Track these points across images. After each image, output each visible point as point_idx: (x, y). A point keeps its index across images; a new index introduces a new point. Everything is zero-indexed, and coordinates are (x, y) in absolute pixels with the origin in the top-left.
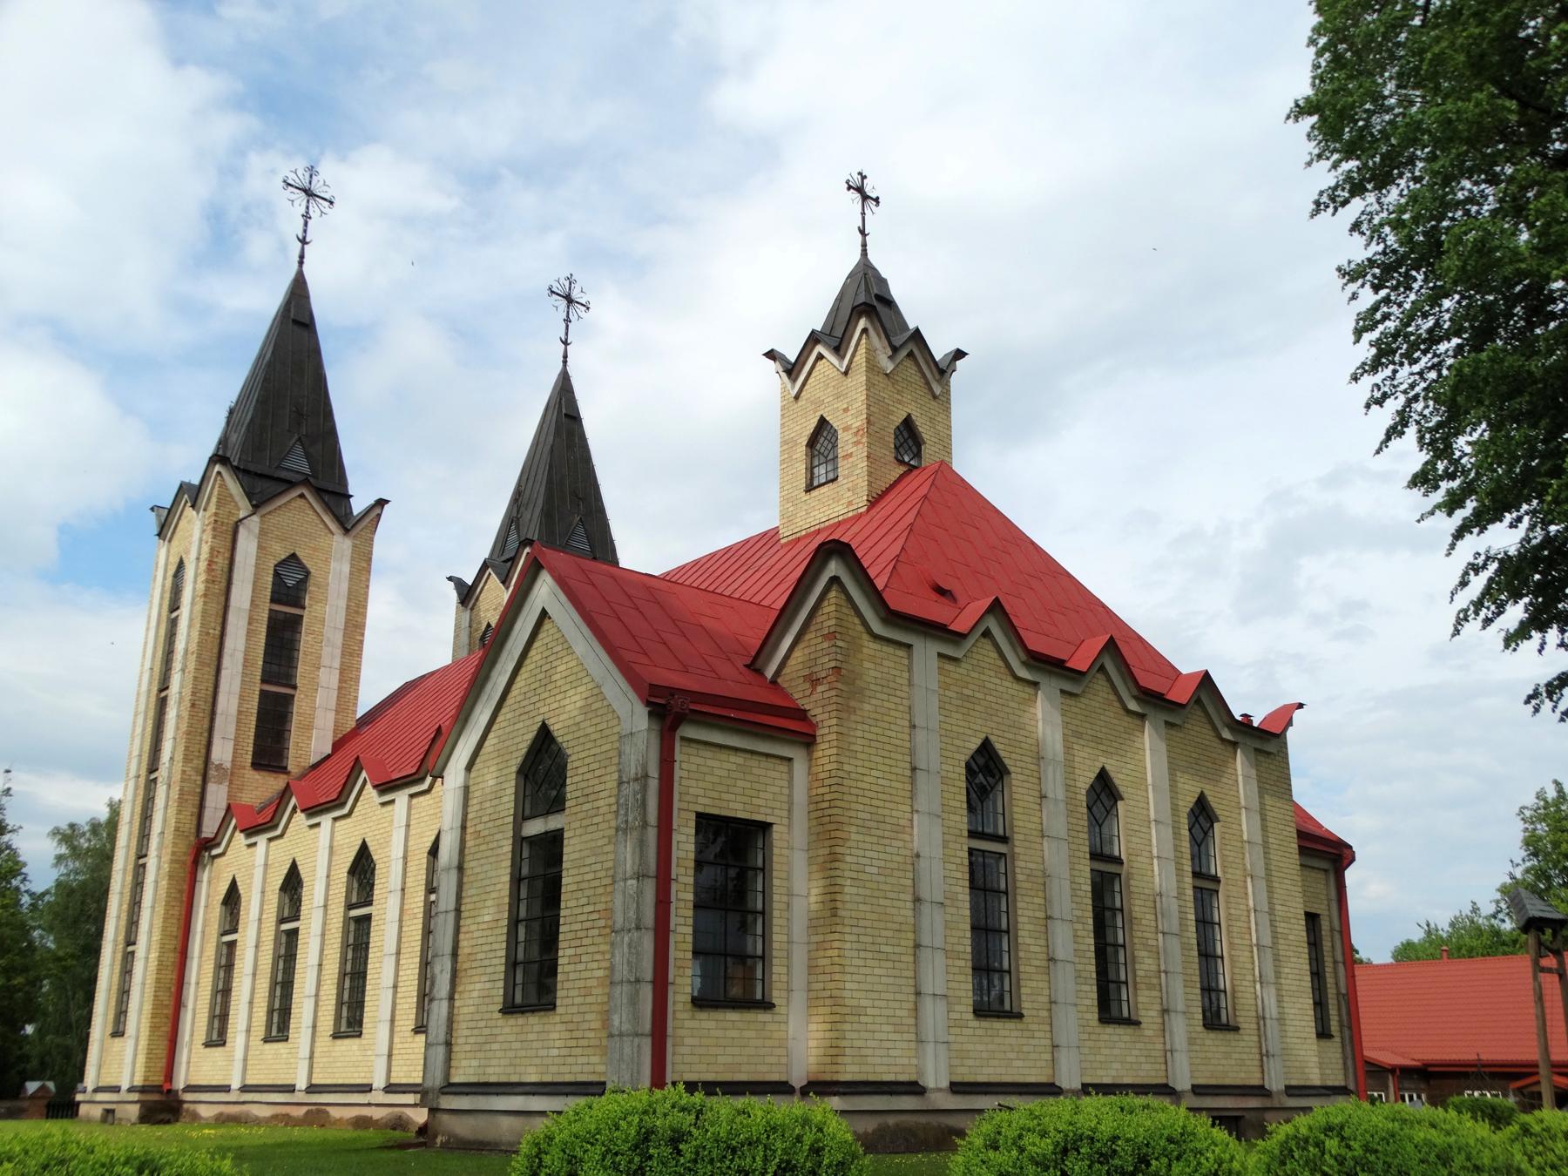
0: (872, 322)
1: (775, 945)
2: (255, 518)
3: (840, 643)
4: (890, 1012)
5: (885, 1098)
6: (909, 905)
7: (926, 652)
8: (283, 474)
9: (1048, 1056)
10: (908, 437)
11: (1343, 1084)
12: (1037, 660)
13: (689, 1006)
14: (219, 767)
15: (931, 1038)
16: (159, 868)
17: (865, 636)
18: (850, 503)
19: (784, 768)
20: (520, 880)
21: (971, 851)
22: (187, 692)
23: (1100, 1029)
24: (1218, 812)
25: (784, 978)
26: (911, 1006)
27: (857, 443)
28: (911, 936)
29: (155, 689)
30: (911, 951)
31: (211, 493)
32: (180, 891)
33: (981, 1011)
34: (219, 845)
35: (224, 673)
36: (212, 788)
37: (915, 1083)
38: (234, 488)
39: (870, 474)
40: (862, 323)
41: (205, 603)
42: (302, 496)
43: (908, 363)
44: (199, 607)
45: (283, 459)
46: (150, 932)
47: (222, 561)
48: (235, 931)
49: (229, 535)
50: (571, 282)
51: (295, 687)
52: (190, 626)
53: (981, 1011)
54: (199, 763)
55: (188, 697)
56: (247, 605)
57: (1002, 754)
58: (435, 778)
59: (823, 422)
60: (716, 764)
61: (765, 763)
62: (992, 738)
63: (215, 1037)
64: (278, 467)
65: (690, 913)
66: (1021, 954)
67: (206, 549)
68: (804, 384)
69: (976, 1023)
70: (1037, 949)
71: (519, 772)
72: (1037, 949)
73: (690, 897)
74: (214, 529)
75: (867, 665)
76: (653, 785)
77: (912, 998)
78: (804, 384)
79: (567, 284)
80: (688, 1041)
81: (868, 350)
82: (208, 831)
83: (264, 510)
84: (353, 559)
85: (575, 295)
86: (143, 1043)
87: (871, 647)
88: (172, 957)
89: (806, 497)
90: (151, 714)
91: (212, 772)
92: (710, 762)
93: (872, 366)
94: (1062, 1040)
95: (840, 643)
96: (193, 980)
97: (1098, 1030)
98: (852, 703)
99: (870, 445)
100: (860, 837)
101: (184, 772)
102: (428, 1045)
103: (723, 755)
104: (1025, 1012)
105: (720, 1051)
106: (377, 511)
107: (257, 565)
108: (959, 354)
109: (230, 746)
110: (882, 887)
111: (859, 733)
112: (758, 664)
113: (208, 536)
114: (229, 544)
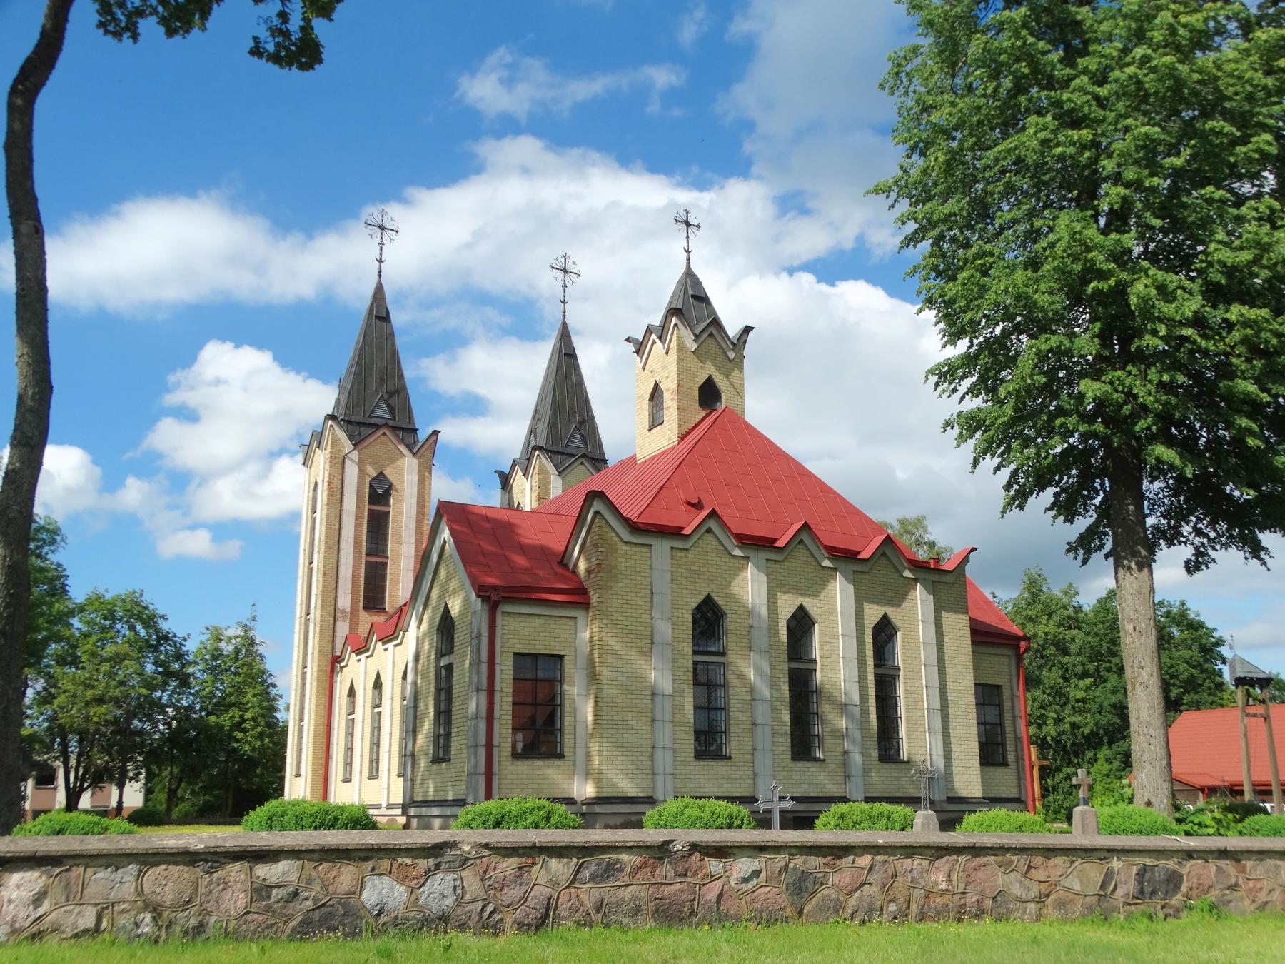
0: (680, 320)
1: (566, 723)
2: (355, 452)
3: (601, 549)
4: (635, 758)
5: (628, 806)
6: (649, 697)
7: (662, 547)
8: (373, 421)
9: (751, 781)
10: (709, 394)
11: (1017, 796)
12: (747, 541)
13: (510, 758)
14: (343, 611)
15: (661, 771)
16: (312, 675)
17: (619, 543)
18: (670, 439)
19: (572, 623)
20: (441, 690)
21: (695, 663)
22: (321, 565)
23: (792, 764)
24: (898, 625)
25: (572, 741)
26: (649, 754)
27: (672, 399)
28: (649, 715)
29: (307, 564)
30: (649, 723)
31: (327, 438)
32: (325, 689)
33: (699, 755)
34: (343, 660)
35: (342, 552)
36: (339, 624)
37: (651, 797)
38: (342, 435)
39: (680, 419)
40: (674, 320)
41: (328, 509)
42: (384, 434)
43: (710, 341)
44: (325, 512)
45: (373, 411)
46: (310, 713)
47: (337, 482)
48: (352, 713)
49: (339, 464)
50: (565, 257)
51: (387, 558)
52: (321, 524)
53: (699, 755)
54: (331, 609)
55: (322, 569)
56: (354, 508)
57: (720, 603)
58: (405, 632)
59: (656, 385)
60: (527, 624)
61: (558, 621)
62: (713, 594)
63: (374, 774)
64: (370, 417)
65: (510, 708)
66: (732, 722)
67: (327, 474)
68: (647, 360)
69: (697, 763)
70: (745, 718)
71: (438, 630)
72: (745, 718)
73: (511, 699)
74: (331, 462)
75: (620, 560)
76: (485, 641)
77: (650, 750)
78: (647, 360)
79: (563, 260)
80: (509, 777)
81: (678, 338)
82: (338, 653)
83: (361, 447)
84: (419, 471)
85: (569, 268)
86: (309, 780)
87: (624, 548)
88: (323, 729)
89: (649, 434)
90: (306, 578)
91: (339, 615)
92: (522, 624)
93: (681, 348)
94: (760, 771)
95: (601, 549)
96: (335, 743)
97: (790, 765)
98: (609, 584)
99: (679, 400)
100: (614, 661)
101: (322, 616)
102: (405, 781)
103: (531, 620)
104: (733, 756)
105: (530, 782)
106: (434, 438)
107: (359, 482)
108: (748, 329)
109: (349, 598)
110: (630, 688)
111: (615, 601)
112: (565, 561)
113: (327, 467)
114: (340, 471)
